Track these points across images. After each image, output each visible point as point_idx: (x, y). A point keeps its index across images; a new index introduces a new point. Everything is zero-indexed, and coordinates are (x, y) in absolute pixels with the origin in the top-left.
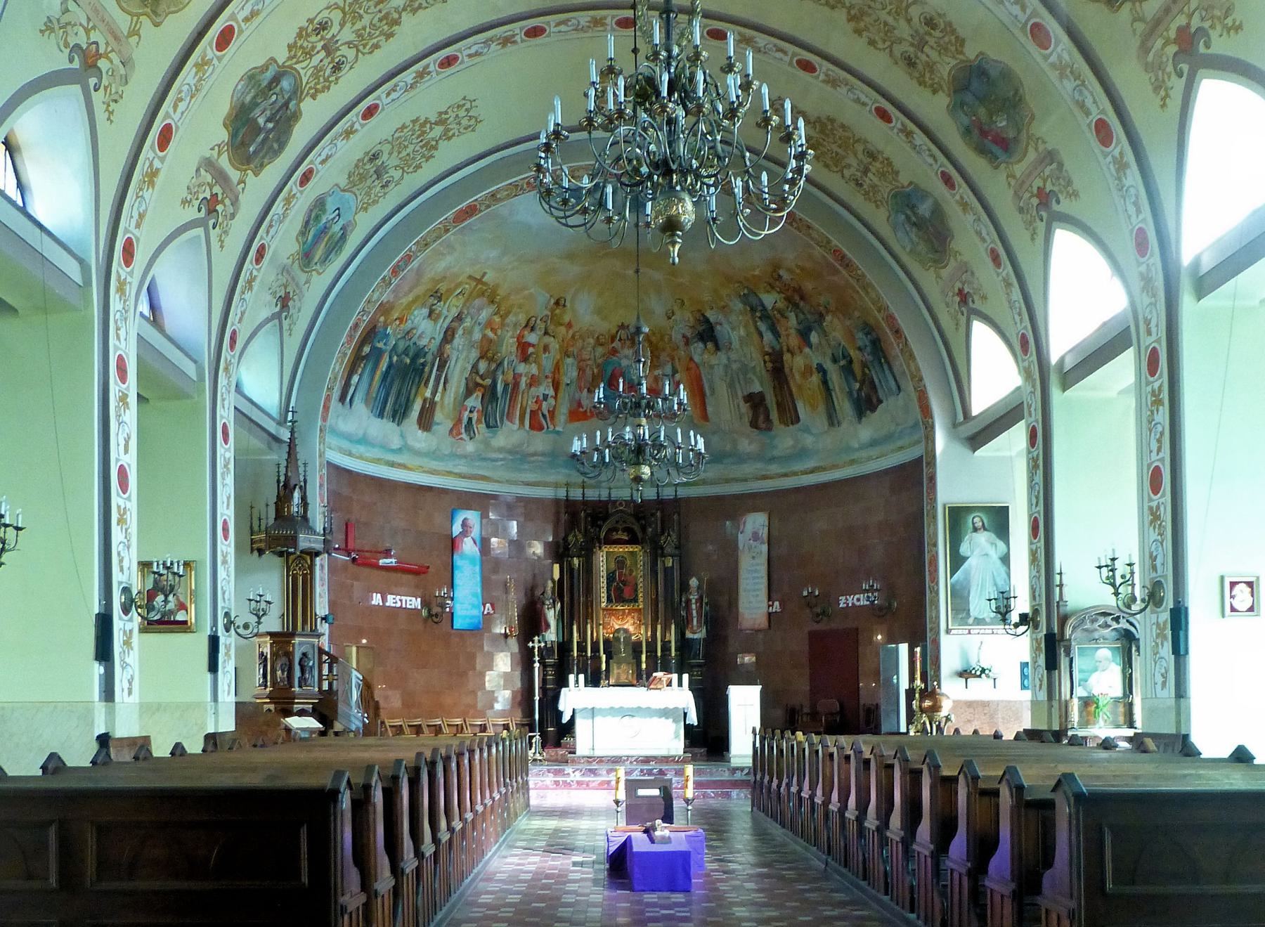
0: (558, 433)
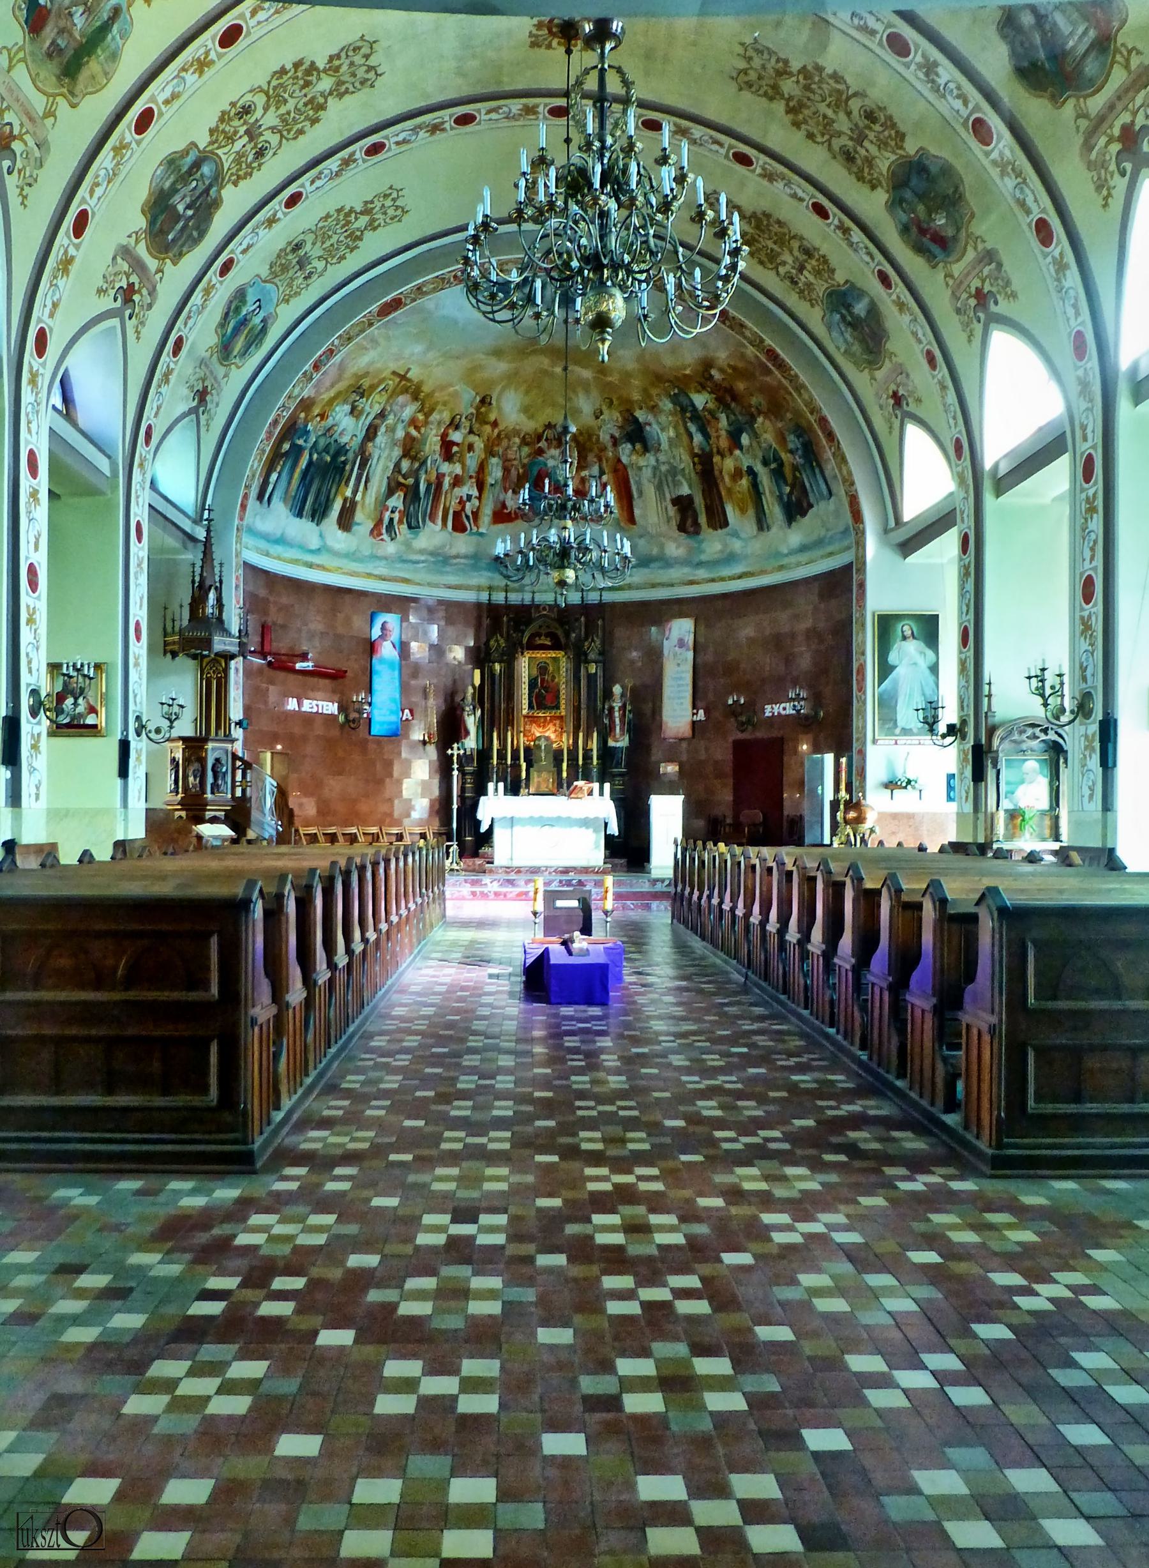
0: (481, 534)
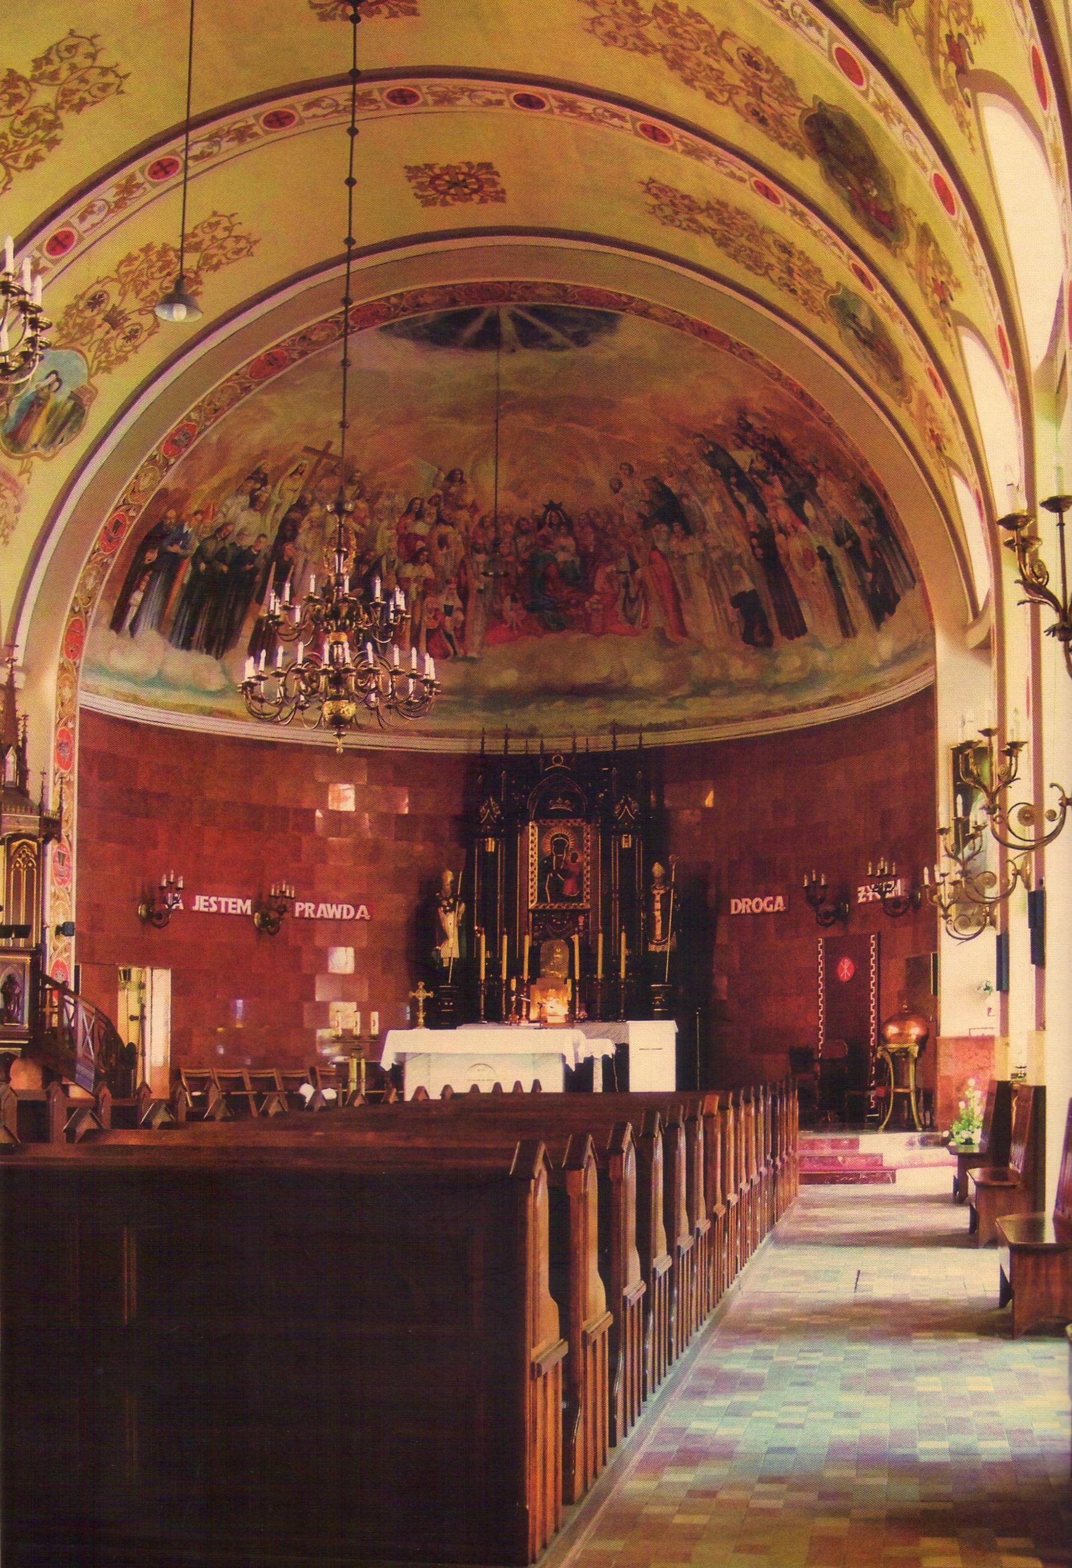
0: (472, 660)
